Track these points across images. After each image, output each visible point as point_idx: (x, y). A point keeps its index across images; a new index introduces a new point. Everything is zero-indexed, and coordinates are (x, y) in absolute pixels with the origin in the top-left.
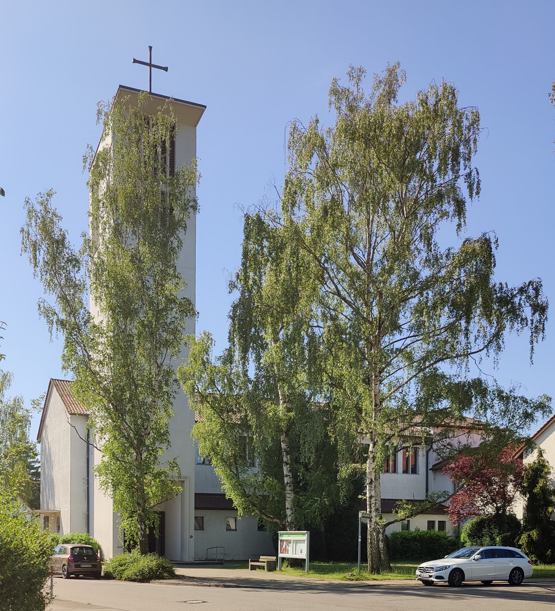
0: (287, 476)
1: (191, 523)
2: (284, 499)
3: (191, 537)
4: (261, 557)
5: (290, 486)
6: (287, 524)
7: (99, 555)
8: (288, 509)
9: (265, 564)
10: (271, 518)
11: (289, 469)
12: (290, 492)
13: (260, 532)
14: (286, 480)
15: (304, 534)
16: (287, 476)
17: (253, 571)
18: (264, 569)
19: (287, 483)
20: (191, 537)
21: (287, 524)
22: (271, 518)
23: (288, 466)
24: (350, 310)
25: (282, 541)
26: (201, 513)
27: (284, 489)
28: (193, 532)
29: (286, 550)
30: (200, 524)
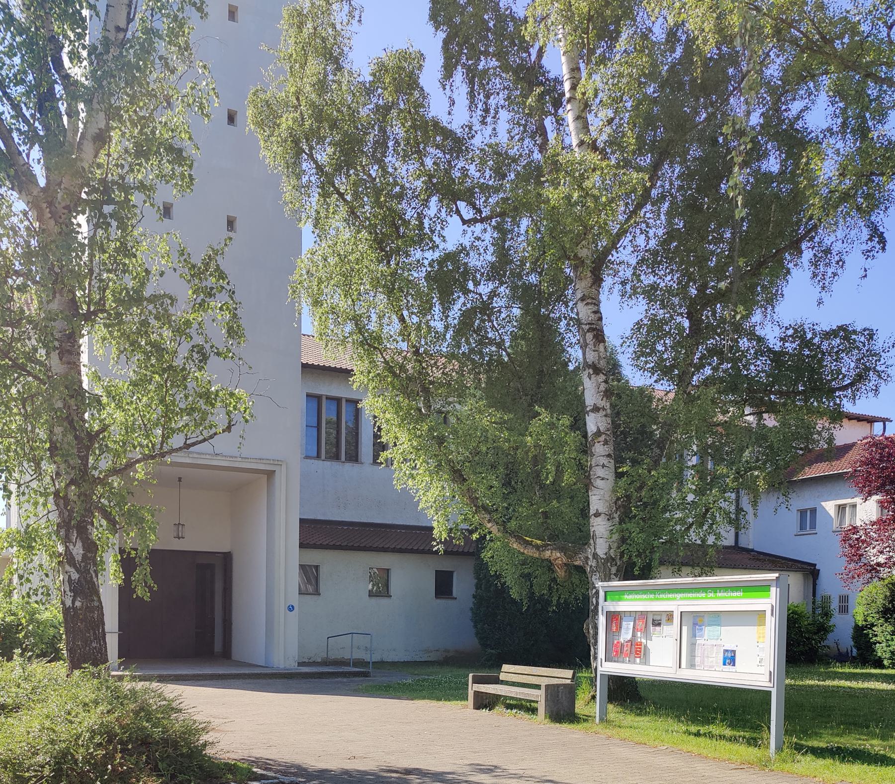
0: (596, 409)
1: (289, 577)
2: (588, 485)
3: (291, 608)
4: (506, 667)
5: (606, 443)
6: (592, 563)
7: (506, 359)
8: (597, 515)
9: (539, 696)
10: (537, 547)
11: (603, 387)
12: (604, 460)
13: (438, 601)
14: (594, 422)
15: (763, 587)
16: (596, 409)
17: (485, 712)
18: (534, 711)
19: (598, 433)
20: (291, 608)
21: (592, 563)
22: (537, 547)
23: (602, 378)
24: (590, 118)
25: (614, 618)
26: (315, 557)
27: (585, 449)
28: (294, 599)
29: (638, 651)
30: (311, 577)
